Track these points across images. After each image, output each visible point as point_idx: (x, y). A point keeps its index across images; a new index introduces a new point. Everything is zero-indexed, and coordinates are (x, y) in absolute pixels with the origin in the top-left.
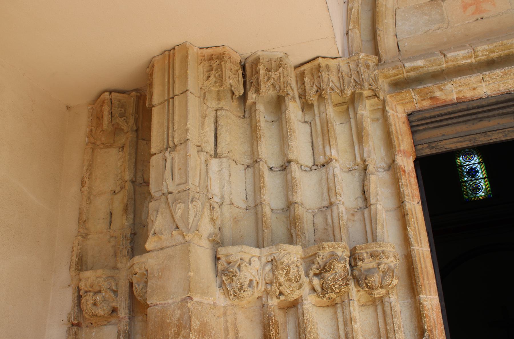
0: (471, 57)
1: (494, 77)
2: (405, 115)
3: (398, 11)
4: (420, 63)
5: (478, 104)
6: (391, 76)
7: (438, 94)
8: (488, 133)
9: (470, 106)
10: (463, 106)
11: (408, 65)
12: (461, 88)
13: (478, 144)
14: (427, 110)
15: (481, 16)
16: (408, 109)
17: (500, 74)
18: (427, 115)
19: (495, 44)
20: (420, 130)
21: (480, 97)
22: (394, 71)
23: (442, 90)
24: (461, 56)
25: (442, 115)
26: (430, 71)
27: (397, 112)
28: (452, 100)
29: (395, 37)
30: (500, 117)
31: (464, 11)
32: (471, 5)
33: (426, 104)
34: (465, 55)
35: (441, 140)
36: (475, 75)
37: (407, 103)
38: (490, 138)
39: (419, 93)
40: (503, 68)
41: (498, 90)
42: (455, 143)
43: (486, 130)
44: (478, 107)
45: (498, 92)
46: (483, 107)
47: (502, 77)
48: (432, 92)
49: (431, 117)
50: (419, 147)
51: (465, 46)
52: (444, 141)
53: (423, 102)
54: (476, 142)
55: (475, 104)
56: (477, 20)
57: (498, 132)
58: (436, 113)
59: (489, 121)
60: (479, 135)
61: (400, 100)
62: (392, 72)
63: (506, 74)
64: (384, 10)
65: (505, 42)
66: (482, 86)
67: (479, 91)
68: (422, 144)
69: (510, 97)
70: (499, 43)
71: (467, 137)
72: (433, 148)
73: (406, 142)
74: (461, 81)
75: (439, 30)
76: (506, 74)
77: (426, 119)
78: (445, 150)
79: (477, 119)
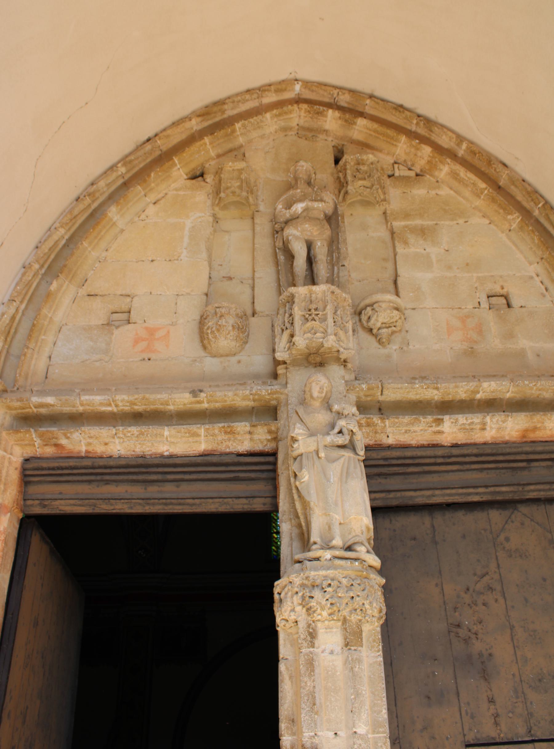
0: (110, 405)
1: (129, 435)
2: (20, 460)
3: (64, 328)
4: (50, 400)
5: (106, 463)
6: (16, 409)
7: (63, 441)
8: (111, 501)
9: (96, 464)
10: (88, 463)
11: (35, 399)
12: (91, 441)
13: (98, 511)
14: (47, 458)
15: (150, 356)
16: (27, 453)
17: (136, 433)
18: (45, 465)
19: (136, 396)
20: (34, 482)
21: (111, 454)
22: (19, 404)
23: (68, 438)
24: (96, 401)
25: (62, 468)
26: (64, 412)
27: (11, 454)
28: (80, 452)
29: (48, 359)
30: (130, 483)
31: (134, 346)
32: (143, 340)
33: (49, 451)
34: (102, 401)
35: (56, 499)
36: (107, 428)
37: (26, 445)
38: (112, 507)
39: (41, 436)
40: (139, 426)
41: (134, 451)
42: (71, 505)
43: (109, 496)
44: (106, 467)
45: (133, 453)
46: (111, 467)
47: (137, 437)
48: (56, 438)
49: (49, 469)
50: (29, 502)
51: (109, 390)
52: (59, 501)
53: (46, 447)
54: (96, 508)
55: (101, 463)
56: (144, 359)
57: (122, 501)
58: (56, 465)
59: (117, 486)
60: (100, 501)
61: (18, 440)
62: (17, 404)
63: (143, 434)
64: (46, 323)
65: (147, 396)
66: (115, 443)
67: (111, 447)
68: (33, 500)
69: (143, 463)
70: (141, 396)
71: (87, 501)
72: (45, 506)
73: (10, 494)
74: (91, 431)
75: (98, 363)
76: (142, 433)
77: (43, 469)
78: (58, 512)
79: (102, 481)
